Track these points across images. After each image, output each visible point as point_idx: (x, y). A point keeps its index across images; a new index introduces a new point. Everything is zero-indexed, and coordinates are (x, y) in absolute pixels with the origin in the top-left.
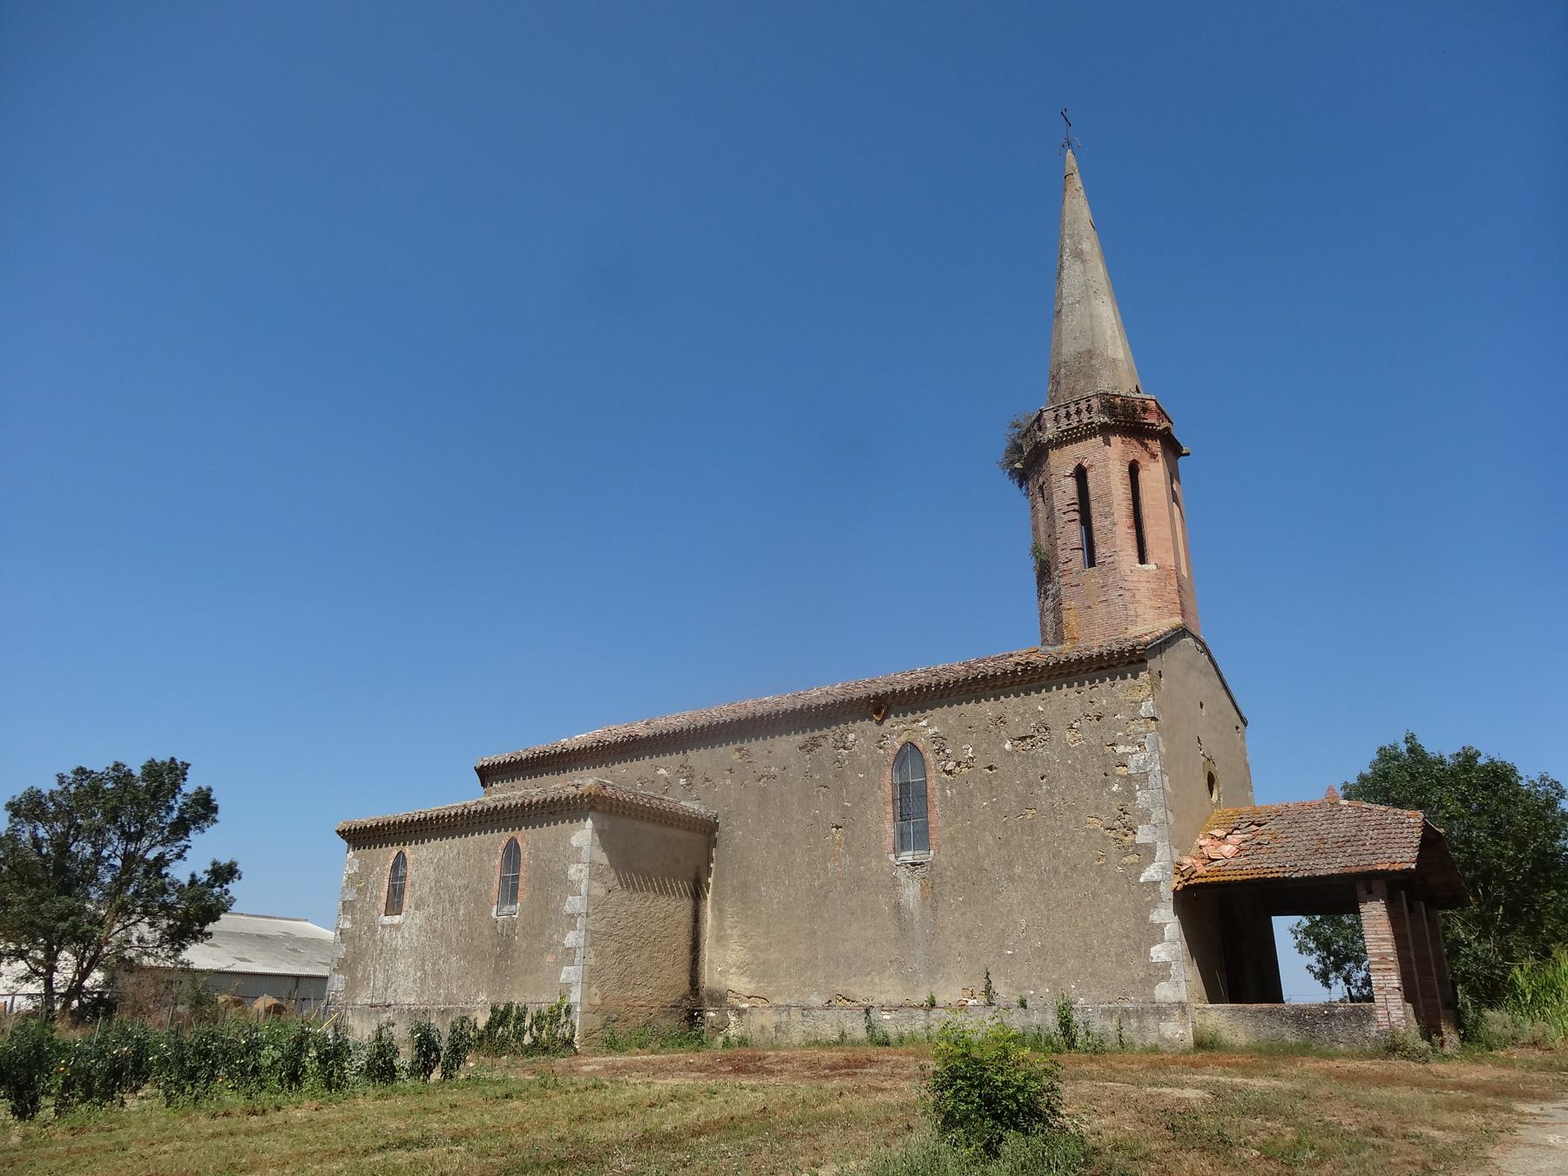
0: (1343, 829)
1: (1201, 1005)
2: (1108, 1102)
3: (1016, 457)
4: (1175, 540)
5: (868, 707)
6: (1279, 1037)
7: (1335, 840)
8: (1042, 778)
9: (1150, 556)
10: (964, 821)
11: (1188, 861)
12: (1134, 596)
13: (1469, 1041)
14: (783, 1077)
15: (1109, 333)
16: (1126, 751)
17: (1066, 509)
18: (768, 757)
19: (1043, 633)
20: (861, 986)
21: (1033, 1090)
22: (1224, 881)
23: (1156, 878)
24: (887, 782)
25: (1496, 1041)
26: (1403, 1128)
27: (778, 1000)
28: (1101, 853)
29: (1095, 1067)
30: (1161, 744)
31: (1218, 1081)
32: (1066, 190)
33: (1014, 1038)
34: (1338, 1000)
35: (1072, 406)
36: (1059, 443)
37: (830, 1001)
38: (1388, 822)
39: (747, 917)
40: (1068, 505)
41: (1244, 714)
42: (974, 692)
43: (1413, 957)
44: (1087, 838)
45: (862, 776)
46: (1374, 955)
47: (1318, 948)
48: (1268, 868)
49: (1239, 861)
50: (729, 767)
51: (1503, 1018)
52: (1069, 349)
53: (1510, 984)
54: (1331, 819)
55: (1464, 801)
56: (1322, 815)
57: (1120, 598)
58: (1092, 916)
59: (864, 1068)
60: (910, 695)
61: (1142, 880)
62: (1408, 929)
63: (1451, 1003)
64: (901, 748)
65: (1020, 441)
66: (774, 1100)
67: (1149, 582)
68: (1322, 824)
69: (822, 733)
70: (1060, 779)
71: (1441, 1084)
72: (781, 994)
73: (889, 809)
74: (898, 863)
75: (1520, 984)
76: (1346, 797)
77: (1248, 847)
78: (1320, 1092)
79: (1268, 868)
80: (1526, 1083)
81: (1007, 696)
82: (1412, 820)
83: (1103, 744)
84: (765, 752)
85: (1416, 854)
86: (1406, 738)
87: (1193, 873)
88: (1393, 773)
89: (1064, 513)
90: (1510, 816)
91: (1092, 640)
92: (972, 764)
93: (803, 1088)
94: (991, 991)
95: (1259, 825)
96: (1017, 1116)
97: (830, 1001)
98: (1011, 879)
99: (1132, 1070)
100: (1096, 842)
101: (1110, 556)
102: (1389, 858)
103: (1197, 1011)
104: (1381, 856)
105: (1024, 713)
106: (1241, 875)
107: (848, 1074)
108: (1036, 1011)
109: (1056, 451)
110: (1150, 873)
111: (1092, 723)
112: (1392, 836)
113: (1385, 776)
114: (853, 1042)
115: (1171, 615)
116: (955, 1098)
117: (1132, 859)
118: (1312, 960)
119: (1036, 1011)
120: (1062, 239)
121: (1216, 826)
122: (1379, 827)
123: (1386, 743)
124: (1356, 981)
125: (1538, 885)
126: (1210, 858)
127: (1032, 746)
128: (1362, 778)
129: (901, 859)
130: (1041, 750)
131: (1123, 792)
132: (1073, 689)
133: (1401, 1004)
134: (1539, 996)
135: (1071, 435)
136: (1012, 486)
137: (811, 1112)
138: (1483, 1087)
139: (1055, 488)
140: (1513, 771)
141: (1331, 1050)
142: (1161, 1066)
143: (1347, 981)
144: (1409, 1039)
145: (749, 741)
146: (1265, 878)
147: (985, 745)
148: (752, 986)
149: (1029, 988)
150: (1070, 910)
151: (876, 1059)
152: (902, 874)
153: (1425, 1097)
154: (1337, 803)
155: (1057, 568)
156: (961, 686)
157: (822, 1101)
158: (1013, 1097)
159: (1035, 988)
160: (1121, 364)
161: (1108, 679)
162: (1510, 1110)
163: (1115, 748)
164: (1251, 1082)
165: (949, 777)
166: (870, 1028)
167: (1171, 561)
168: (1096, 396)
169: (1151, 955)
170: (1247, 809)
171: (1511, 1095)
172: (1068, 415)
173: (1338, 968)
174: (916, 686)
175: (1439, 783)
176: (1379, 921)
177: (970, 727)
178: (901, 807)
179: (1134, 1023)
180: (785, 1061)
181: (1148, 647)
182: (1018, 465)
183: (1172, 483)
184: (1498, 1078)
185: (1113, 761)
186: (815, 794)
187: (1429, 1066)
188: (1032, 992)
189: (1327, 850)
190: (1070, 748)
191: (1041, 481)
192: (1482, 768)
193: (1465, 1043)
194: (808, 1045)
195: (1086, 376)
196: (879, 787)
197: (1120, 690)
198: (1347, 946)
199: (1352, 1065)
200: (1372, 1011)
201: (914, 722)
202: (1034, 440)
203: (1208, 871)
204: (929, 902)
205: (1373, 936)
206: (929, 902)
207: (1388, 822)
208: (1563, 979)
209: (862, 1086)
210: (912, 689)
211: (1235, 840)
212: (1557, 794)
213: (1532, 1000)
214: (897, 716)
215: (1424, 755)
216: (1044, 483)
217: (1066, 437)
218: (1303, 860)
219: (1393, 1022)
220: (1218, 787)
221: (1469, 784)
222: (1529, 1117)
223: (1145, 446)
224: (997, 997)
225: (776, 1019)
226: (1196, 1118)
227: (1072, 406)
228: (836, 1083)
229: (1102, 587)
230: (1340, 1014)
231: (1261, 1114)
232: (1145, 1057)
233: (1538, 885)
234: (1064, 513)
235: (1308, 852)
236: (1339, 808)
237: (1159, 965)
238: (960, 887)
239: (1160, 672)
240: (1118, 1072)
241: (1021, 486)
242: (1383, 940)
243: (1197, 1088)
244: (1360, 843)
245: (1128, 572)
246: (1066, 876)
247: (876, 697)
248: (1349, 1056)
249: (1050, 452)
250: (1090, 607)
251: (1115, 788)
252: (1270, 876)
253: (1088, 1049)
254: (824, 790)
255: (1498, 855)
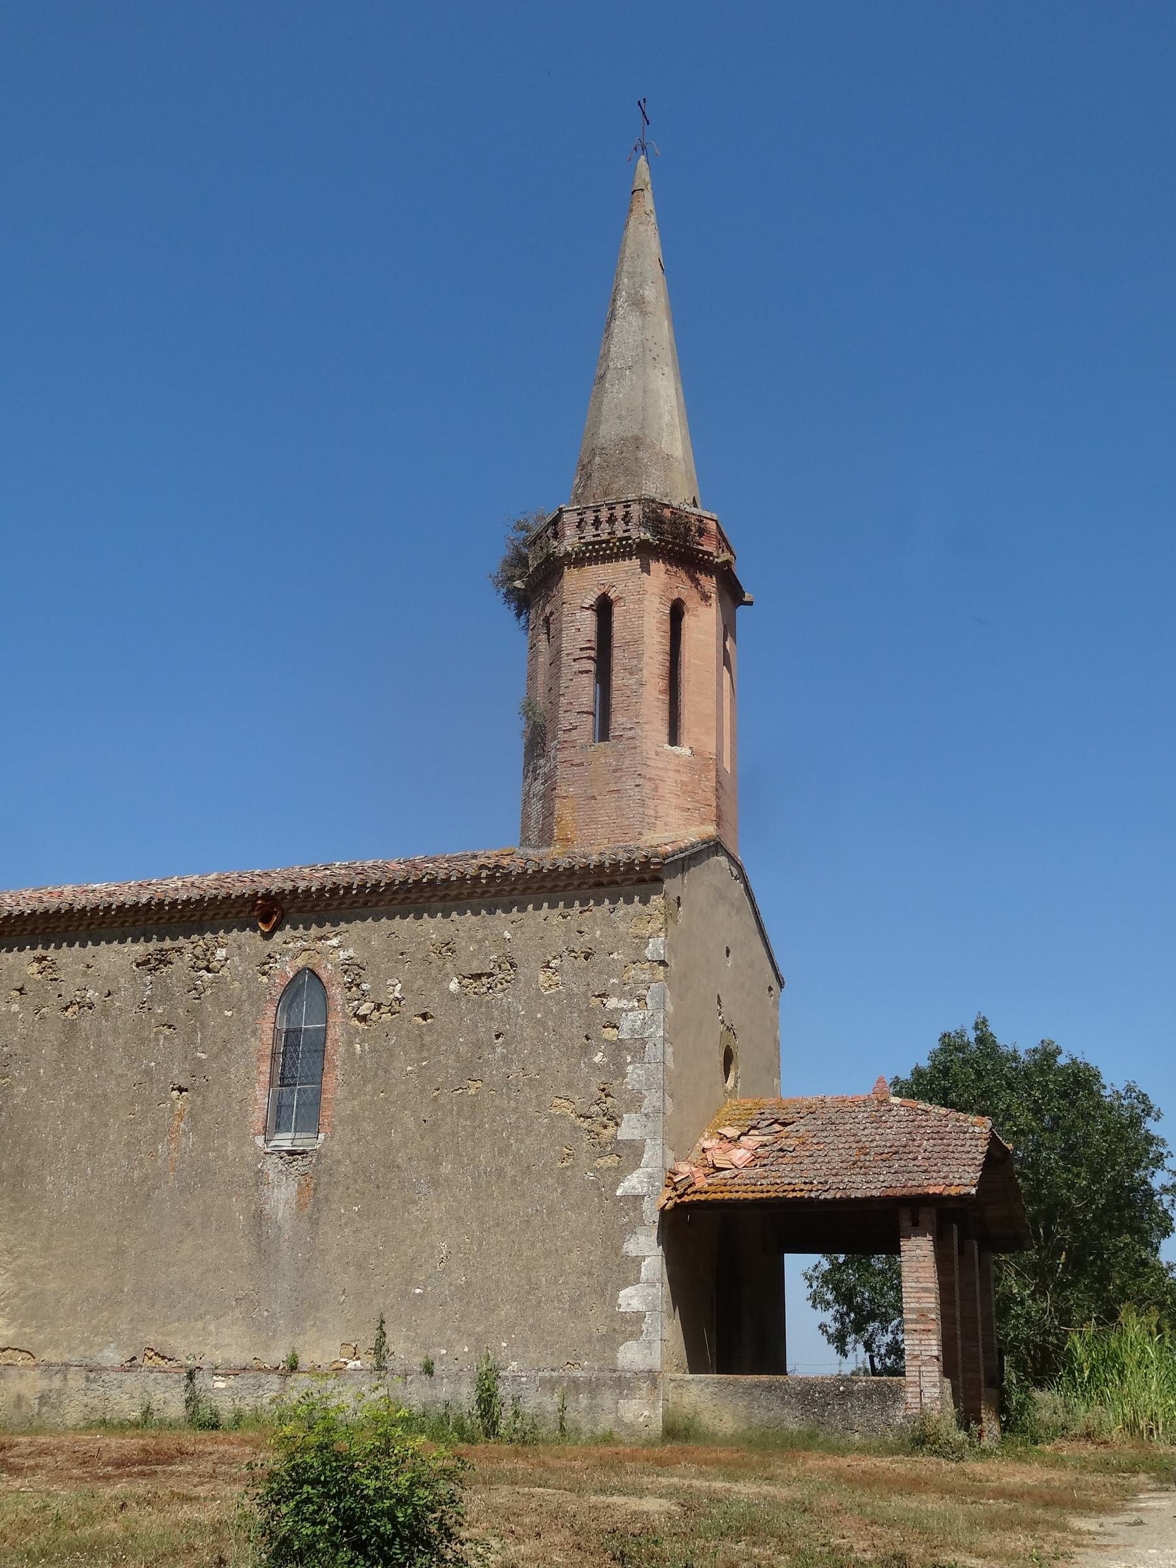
0: (891, 1136)
1: (679, 1376)
2: (533, 1519)
3: (518, 572)
4: (720, 707)
5: (252, 911)
6: (777, 1422)
7: (880, 1150)
8: (498, 1037)
9: (684, 736)
10: (375, 1093)
11: (685, 1169)
12: (656, 789)
13: (1010, 1431)
14: (35, 1478)
15: (666, 418)
16: (619, 1006)
17: (578, 654)
18: (84, 974)
19: (525, 828)
20: (186, 1337)
21: (422, 1502)
22: (730, 1199)
23: (639, 1190)
24: (267, 1027)
25: (1042, 1432)
26: (932, 1555)
27: (50, 1356)
28: (567, 1151)
29: (521, 1464)
30: (668, 1000)
31: (690, 1486)
32: (631, 211)
33: (407, 1421)
34: (849, 1373)
35: (604, 510)
36: (580, 560)
37: (134, 1358)
38: (947, 1129)
39: (16, 1222)
40: (581, 649)
41: (782, 972)
42: (415, 902)
43: (958, 1314)
44: (550, 1127)
45: (229, 1014)
46: (912, 1310)
47: (836, 1300)
48: (789, 1184)
49: (752, 1173)
50: (19, 985)
51: (1054, 1400)
52: (609, 430)
53: (1066, 1356)
54: (878, 1121)
55: (1037, 1111)
56: (866, 1115)
57: (637, 789)
58: (543, 1241)
59: (170, 1464)
60: (318, 898)
61: (619, 1193)
62: (956, 1279)
63: (995, 1380)
64: (295, 976)
65: (525, 551)
66: (8, 1517)
67: (679, 771)
68: (865, 1128)
69: (177, 944)
70: (523, 1039)
71: (976, 1490)
72: (56, 1346)
73: (265, 1067)
74: (269, 1150)
75: (1078, 1356)
76: (897, 1094)
77: (767, 1154)
78: (827, 1502)
79: (789, 1184)
80: (1080, 1488)
81: (462, 913)
82: (977, 1130)
83: (590, 994)
84: (82, 967)
85: (978, 1175)
86: (977, 1023)
87: (690, 1186)
88: (955, 1069)
89: (575, 660)
90: (1087, 1135)
91: (591, 844)
92: (397, 1008)
93: (64, 1497)
94: (384, 1349)
95: (785, 1124)
96: (390, 1544)
97: (134, 1358)
98: (434, 1183)
99: (572, 1470)
100: (562, 1135)
101: (631, 729)
102: (944, 1178)
103: (672, 1384)
104: (935, 1175)
105: (483, 940)
106: (753, 1192)
107: (142, 1474)
108: (445, 1380)
109: (575, 571)
110: (633, 1183)
111: (578, 963)
112: (951, 1148)
113: (945, 1072)
114: (161, 1423)
115: (703, 821)
116: (297, 1515)
117: (610, 1161)
118: (827, 1317)
119: (445, 1380)
120: (618, 276)
121: (728, 1123)
122: (936, 1136)
123: (951, 1029)
124: (879, 1347)
125: (1110, 1227)
126: (714, 1167)
127: (489, 989)
128: (918, 1073)
129: (273, 1143)
130: (500, 995)
131: (608, 1065)
132: (556, 911)
133: (937, 1379)
134: (1099, 1372)
135: (597, 551)
136: (507, 613)
137: (66, 1536)
138: (1030, 1494)
139: (566, 622)
140: (1097, 1076)
141: (842, 1443)
142: (614, 1464)
143: (868, 1347)
144: (942, 1427)
145: (58, 947)
146: (785, 1198)
147: (420, 982)
148: (10, 1332)
149: (440, 1345)
150: (513, 1232)
151: (191, 1449)
152: (272, 1167)
153: (960, 1509)
154: (886, 1101)
155: (555, 737)
156: (396, 892)
157: (89, 1518)
158: (390, 1515)
159: (449, 1345)
160: (677, 464)
161: (607, 901)
162: (1064, 1528)
163: (605, 1001)
164: (736, 1487)
165: (362, 1026)
166: (192, 1401)
167: (710, 747)
168: (639, 501)
169: (620, 1301)
170: (773, 1101)
171: (1063, 1506)
172: (597, 523)
173: (858, 1328)
174: (329, 886)
175: (1010, 1086)
176: (922, 1265)
177: (402, 954)
178: (284, 1066)
179: (584, 1400)
180: (43, 1451)
181: (666, 862)
182: (518, 584)
183: (725, 640)
184: (1047, 1481)
185: (601, 1019)
186: (152, 1036)
187: (963, 1464)
188: (444, 1352)
189: (867, 1163)
190: (543, 996)
191: (548, 609)
192: (1062, 1070)
193: (1007, 1434)
194: (89, 1427)
195: (627, 471)
196: (254, 1033)
197: (623, 919)
198: (874, 1299)
199: (867, 1463)
200: (901, 1388)
201: (320, 939)
202: (545, 551)
203: (710, 1185)
204: (307, 1211)
205: (913, 1285)
206: (307, 1211)
207: (947, 1129)
208: (1129, 1350)
209: (160, 1493)
210: (321, 890)
211: (750, 1143)
212: (1143, 1111)
213: (1089, 1377)
214: (295, 928)
215: (995, 1047)
216: (552, 614)
217: (591, 552)
218: (836, 1175)
219: (926, 1404)
220: (737, 1068)
221: (1044, 1088)
222: (1087, 1537)
223: (696, 582)
224: (392, 1357)
225: (43, 1384)
226: (656, 1542)
227: (604, 510)
228: (121, 1487)
229: (615, 771)
230: (859, 1391)
231: (745, 1534)
232: (594, 1451)
233: (1110, 1227)
234: (575, 660)
235: (844, 1165)
236: (887, 1108)
237: (628, 1316)
238: (357, 1191)
239: (679, 898)
240: (553, 1471)
241: (518, 615)
242: (925, 1290)
243: (661, 1497)
244: (910, 1156)
245: (652, 754)
246: (514, 1182)
247: (267, 896)
248: (861, 1450)
249: (566, 570)
250: (594, 798)
251: (598, 1058)
252: (791, 1195)
253: (514, 1437)
254: (167, 1032)
255: (1068, 1185)
